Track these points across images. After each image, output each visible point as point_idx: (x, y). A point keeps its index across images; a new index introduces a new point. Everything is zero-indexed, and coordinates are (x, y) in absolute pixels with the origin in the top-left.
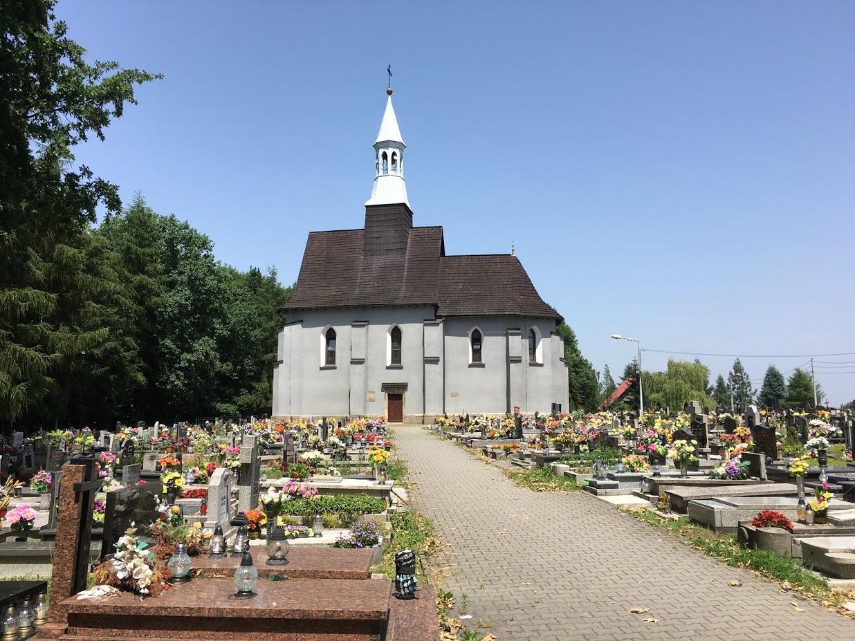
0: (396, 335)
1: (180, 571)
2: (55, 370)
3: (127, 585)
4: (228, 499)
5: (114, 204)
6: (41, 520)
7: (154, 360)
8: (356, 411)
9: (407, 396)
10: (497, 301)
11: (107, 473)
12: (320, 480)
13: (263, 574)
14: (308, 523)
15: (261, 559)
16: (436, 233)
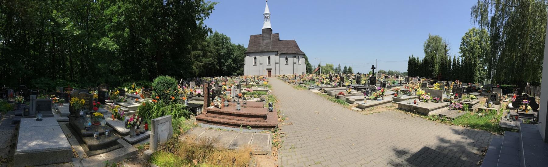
0: (269, 58)
1: (226, 105)
2: (203, 66)
3: (217, 106)
4: (235, 92)
5: (211, 32)
6: (202, 94)
7: (221, 64)
8: (261, 74)
9: (272, 71)
10: (291, 50)
11: (213, 86)
12: (253, 88)
13: (242, 106)
14: (251, 97)
15: (241, 104)
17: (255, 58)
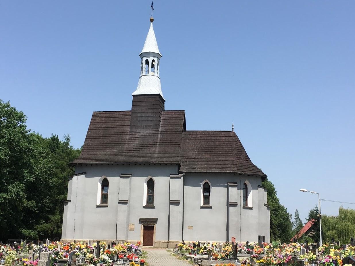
0: (151, 184)
8: (121, 237)
10: (221, 163)
16: (181, 114)
17: (105, 184)
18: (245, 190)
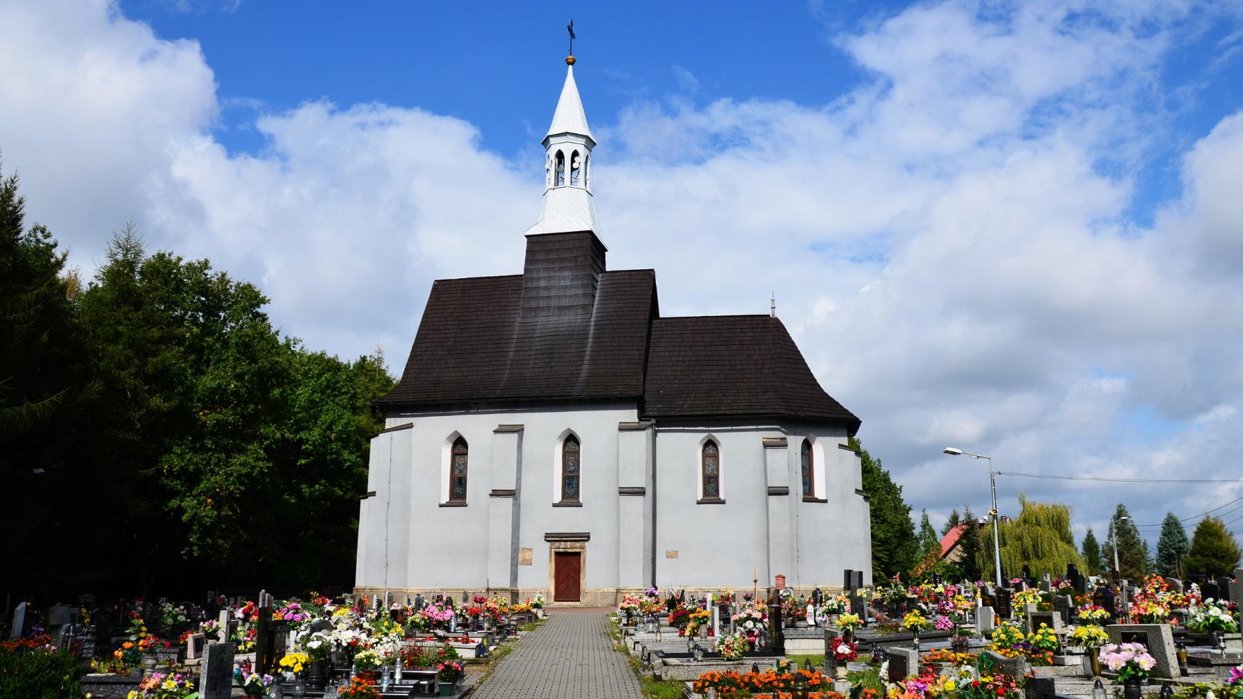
16: (646, 280)
18: (661, 437)
